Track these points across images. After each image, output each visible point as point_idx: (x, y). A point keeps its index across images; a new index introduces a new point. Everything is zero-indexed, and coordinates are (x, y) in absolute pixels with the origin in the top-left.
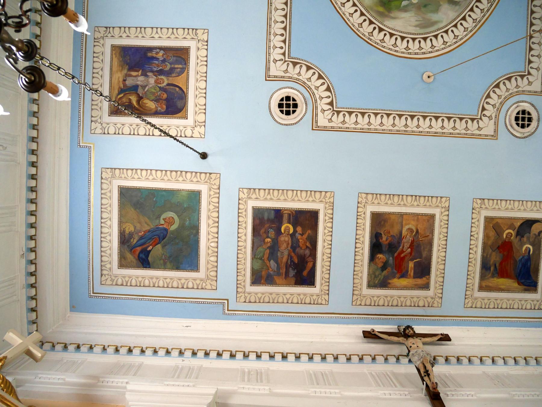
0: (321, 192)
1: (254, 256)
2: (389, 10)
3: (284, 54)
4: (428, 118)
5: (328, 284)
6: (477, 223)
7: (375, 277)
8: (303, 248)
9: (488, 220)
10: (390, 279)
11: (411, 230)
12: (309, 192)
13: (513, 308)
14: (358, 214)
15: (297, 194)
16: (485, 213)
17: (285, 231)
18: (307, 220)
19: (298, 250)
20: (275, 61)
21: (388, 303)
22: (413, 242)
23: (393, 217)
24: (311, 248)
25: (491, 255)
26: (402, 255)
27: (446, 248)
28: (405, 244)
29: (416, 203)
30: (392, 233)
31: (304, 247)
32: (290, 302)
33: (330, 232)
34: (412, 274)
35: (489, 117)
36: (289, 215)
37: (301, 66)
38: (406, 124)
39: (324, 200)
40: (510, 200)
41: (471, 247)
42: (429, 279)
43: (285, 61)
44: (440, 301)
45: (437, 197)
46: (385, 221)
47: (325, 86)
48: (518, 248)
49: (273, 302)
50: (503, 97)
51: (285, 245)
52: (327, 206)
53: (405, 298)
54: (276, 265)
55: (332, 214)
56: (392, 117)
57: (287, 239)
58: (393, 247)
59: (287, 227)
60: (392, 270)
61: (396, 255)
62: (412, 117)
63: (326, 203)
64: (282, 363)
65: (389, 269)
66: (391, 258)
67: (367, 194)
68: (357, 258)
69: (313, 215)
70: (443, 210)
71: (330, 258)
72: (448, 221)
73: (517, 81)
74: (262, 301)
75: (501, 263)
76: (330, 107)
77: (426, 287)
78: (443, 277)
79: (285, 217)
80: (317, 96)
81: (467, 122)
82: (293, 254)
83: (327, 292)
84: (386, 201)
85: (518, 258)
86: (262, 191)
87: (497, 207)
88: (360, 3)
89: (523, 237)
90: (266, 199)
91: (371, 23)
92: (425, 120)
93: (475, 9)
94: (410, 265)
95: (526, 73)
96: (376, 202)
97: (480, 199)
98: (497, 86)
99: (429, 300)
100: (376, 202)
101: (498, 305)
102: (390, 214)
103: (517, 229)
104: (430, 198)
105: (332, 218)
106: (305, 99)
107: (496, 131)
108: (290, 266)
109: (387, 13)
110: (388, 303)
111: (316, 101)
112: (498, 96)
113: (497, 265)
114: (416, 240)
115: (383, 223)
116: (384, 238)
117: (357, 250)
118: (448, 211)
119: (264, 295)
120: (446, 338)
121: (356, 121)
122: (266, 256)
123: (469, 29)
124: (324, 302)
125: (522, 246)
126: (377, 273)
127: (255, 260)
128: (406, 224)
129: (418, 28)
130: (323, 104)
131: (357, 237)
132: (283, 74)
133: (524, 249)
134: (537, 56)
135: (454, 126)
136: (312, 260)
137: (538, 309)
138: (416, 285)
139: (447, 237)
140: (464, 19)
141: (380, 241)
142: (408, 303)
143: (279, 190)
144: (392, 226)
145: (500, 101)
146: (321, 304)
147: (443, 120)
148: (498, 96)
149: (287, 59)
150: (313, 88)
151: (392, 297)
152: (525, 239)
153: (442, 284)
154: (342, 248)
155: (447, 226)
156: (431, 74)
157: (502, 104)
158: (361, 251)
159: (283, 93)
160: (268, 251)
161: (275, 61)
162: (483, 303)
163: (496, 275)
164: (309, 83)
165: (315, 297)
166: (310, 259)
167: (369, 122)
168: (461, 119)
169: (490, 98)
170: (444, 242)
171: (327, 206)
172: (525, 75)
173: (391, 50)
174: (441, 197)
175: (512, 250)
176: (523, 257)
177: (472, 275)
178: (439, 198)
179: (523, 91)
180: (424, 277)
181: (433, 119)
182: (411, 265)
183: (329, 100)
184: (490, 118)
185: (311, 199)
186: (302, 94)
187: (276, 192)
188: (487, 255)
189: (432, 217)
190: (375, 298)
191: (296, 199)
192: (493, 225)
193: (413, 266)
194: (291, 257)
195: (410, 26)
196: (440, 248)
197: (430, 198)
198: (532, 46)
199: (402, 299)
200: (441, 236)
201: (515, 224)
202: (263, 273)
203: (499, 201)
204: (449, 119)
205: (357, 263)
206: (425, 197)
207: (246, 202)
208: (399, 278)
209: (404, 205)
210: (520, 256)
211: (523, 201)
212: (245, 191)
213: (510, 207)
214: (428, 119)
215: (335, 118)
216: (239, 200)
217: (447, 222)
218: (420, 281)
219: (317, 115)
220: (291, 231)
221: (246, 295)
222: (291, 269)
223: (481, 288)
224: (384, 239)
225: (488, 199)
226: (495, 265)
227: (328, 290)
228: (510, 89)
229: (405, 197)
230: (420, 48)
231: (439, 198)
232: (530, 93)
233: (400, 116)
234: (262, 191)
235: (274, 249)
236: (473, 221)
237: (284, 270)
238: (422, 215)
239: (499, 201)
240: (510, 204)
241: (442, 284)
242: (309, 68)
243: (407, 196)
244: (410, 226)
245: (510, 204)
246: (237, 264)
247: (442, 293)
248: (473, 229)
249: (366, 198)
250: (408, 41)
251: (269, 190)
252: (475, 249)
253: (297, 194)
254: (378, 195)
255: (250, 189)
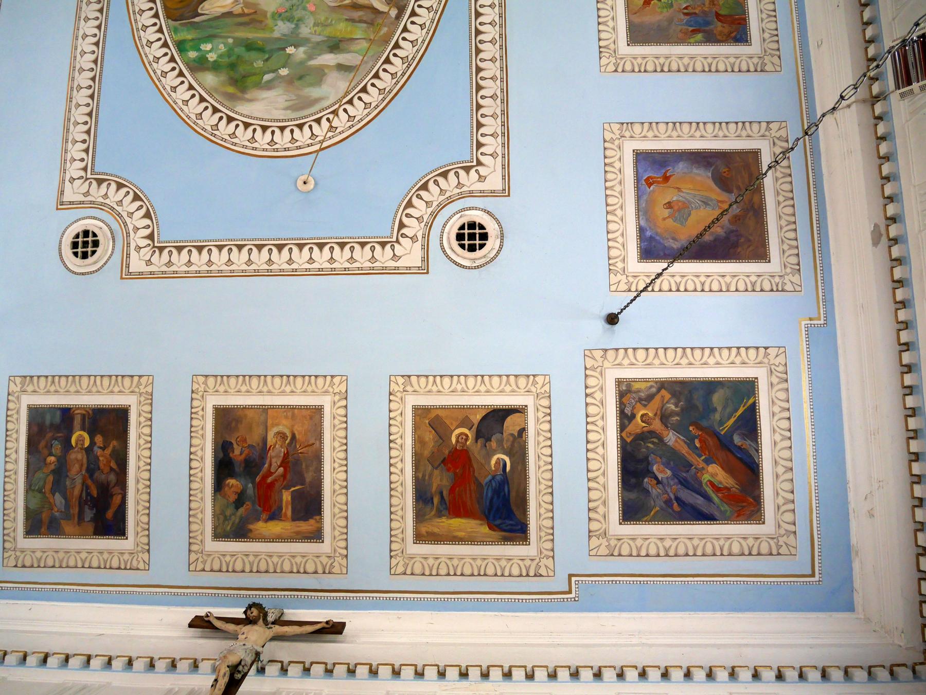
0: (132, 376)
1: (29, 488)
2: (244, 90)
3: (85, 169)
4: (266, 248)
5: (147, 533)
6: (399, 418)
7: (226, 519)
8: (105, 472)
9: (420, 412)
10: (252, 523)
11: (282, 435)
12: (114, 378)
13: (485, 575)
14: (193, 410)
15: (95, 381)
16: (413, 400)
17: (77, 444)
18: (111, 423)
19: (97, 475)
20: (72, 180)
21: (251, 568)
22: (286, 455)
23: (250, 414)
24: (117, 470)
25: (431, 475)
26: (269, 480)
27: (346, 465)
28: (274, 460)
29: (288, 389)
30: (249, 442)
31: (107, 470)
32: (87, 565)
33: (147, 442)
34: (289, 513)
35: (411, 238)
36: (83, 416)
37: (109, 184)
38: (270, 259)
39: (137, 390)
40: (459, 376)
41: (392, 461)
42: (320, 521)
43: (87, 179)
44: (344, 562)
45: (325, 376)
46: (238, 421)
47: (142, 212)
48: (483, 461)
49: (61, 567)
50: (435, 204)
51: (77, 467)
52: (142, 399)
53: (281, 556)
54: (63, 501)
55: (151, 413)
56: (245, 249)
57: (79, 456)
58: (252, 466)
59: (80, 437)
60: (253, 504)
61: (258, 479)
62: (280, 247)
63: (141, 394)
64: (39, 670)
65: (248, 505)
66: (250, 485)
67: (206, 376)
68: (194, 486)
69: (120, 416)
70: (337, 398)
71: (149, 487)
72: (346, 416)
73: (458, 178)
74: (42, 565)
75: (452, 490)
76: (149, 242)
77: (317, 536)
78: (346, 518)
79: (77, 421)
80: (131, 227)
81: (373, 249)
82: (89, 482)
83: (147, 547)
84: (238, 386)
85: (485, 480)
86: (43, 380)
87: (435, 389)
88: (200, 85)
89: (489, 439)
90: (48, 392)
91: (216, 110)
92: (200, 253)
93: (381, 74)
94: (284, 498)
95: (475, 163)
96: (222, 389)
97: (403, 376)
98: (425, 187)
99: (324, 560)
100: (222, 389)
101: (455, 569)
102: (245, 408)
103: (475, 426)
104: (313, 378)
105: (151, 420)
106: (112, 233)
107: (426, 259)
108: (86, 502)
109: (239, 94)
110: (251, 568)
111: (128, 234)
112: (426, 202)
113: (445, 493)
114: (291, 453)
115: (233, 424)
116: (237, 451)
117: (192, 472)
118: (346, 398)
119: (46, 554)
120: (335, 629)
121: (189, 261)
122: (48, 487)
123: (373, 105)
124: (141, 566)
125: (489, 456)
126: (228, 512)
127: (30, 492)
128: (273, 425)
129: (289, 112)
130: (138, 239)
131: (193, 450)
132: (82, 198)
133: (493, 462)
134: (491, 135)
135: (352, 257)
136: (120, 491)
137: (535, 575)
138: (298, 533)
139: (346, 444)
140: (364, 90)
141: (231, 455)
142: (287, 567)
143: (67, 377)
144: (250, 428)
145: (430, 210)
146: (138, 569)
147: (290, 250)
148: (426, 202)
149: (89, 176)
150: (125, 215)
151: (256, 556)
152: (494, 444)
153: (345, 531)
154: (169, 472)
155: (345, 425)
156: (304, 178)
157: (434, 215)
158: (199, 475)
159: (78, 227)
160: (51, 478)
161: (72, 180)
162: (426, 566)
163: (445, 512)
164: (119, 209)
165: (126, 557)
166: (117, 490)
167: (210, 260)
168: (363, 245)
169: (413, 207)
170: (342, 455)
171: (142, 399)
172: (472, 167)
173: (246, 147)
174: (332, 377)
175: (471, 465)
176: (494, 477)
177: (400, 513)
178: (329, 378)
179: (471, 192)
180: (311, 518)
181: (316, 249)
182: (286, 496)
183: (147, 232)
184: (414, 239)
185: (116, 389)
186: (108, 225)
187: (63, 380)
188: (424, 476)
189: (319, 410)
190: (228, 558)
191: (94, 389)
192: (430, 421)
193: (289, 498)
194: (88, 487)
195: (276, 109)
196: (336, 465)
197: (313, 378)
198: (482, 120)
199: (275, 559)
200: (337, 444)
201: (472, 417)
202: (44, 515)
203: (438, 379)
204: (342, 245)
205: (194, 495)
206: (304, 376)
207: (18, 398)
208: (266, 521)
209: (269, 392)
210: (485, 477)
211: (482, 376)
212: (18, 380)
213: (459, 387)
214: (306, 248)
215: (155, 259)
216: (9, 394)
217: (345, 419)
218: (305, 526)
219: (128, 256)
220: (87, 443)
221: (18, 554)
222: (86, 507)
223: (419, 538)
224: (237, 452)
225: (418, 376)
226: (441, 493)
227: (148, 544)
228: (446, 191)
229: (269, 378)
230: (293, 140)
231: (329, 378)
232: (483, 194)
233: (260, 247)
234: (43, 380)
235: (60, 472)
236: (392, 415)
237: (77, 510)
238: (300, 408)
239: (438, 379)
240: (459, 381)
241: (345, 531)
242: (120, 186)
243: (273, 376)
244: (280, 428)
245: (459, 381)
246: (4, 501)
247: (346, 548)
248: (393, 429)
249: (205, 383)
250: (273, 133)
251: (54, 376)
252: (399, 465)
253: (95, 381)
254: (225, 378)
255: (25, 377)
